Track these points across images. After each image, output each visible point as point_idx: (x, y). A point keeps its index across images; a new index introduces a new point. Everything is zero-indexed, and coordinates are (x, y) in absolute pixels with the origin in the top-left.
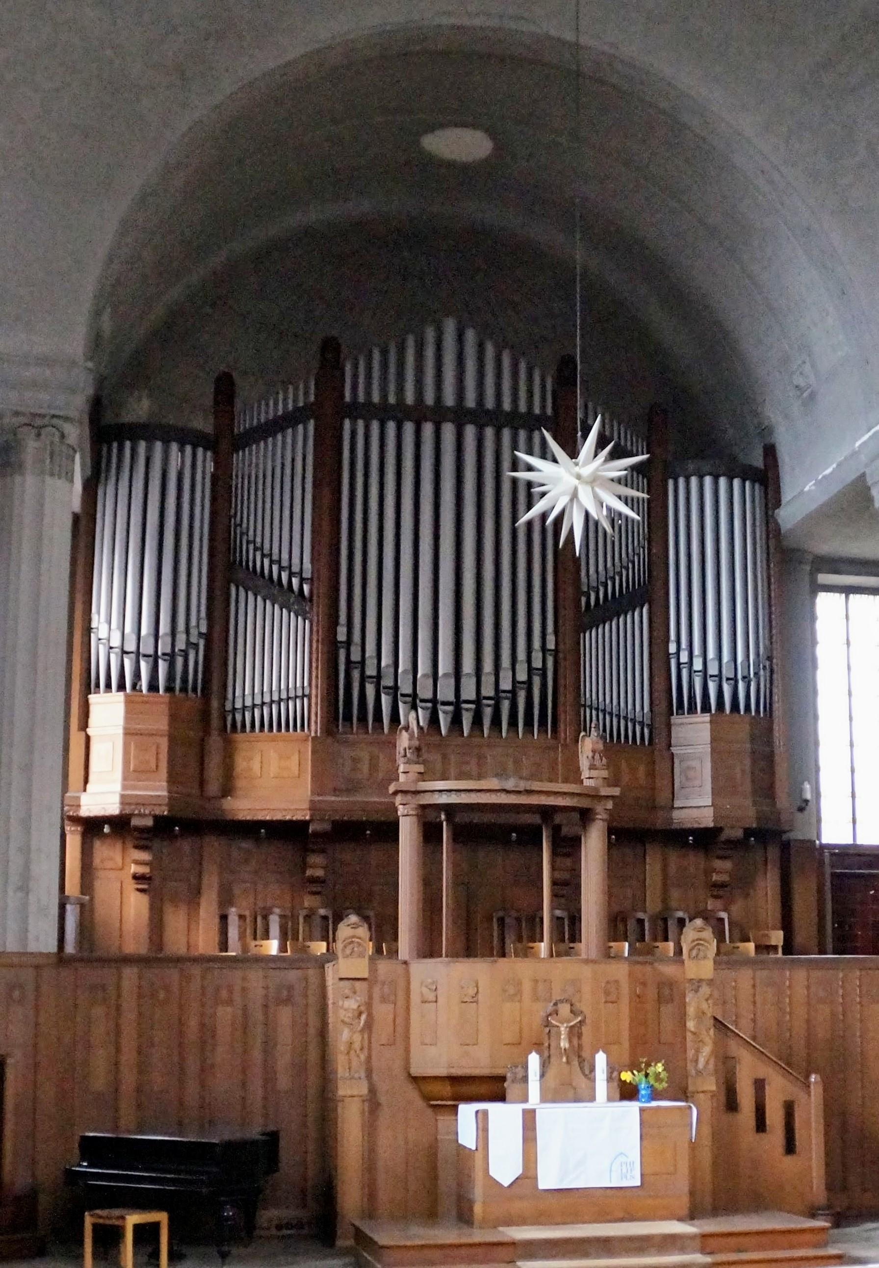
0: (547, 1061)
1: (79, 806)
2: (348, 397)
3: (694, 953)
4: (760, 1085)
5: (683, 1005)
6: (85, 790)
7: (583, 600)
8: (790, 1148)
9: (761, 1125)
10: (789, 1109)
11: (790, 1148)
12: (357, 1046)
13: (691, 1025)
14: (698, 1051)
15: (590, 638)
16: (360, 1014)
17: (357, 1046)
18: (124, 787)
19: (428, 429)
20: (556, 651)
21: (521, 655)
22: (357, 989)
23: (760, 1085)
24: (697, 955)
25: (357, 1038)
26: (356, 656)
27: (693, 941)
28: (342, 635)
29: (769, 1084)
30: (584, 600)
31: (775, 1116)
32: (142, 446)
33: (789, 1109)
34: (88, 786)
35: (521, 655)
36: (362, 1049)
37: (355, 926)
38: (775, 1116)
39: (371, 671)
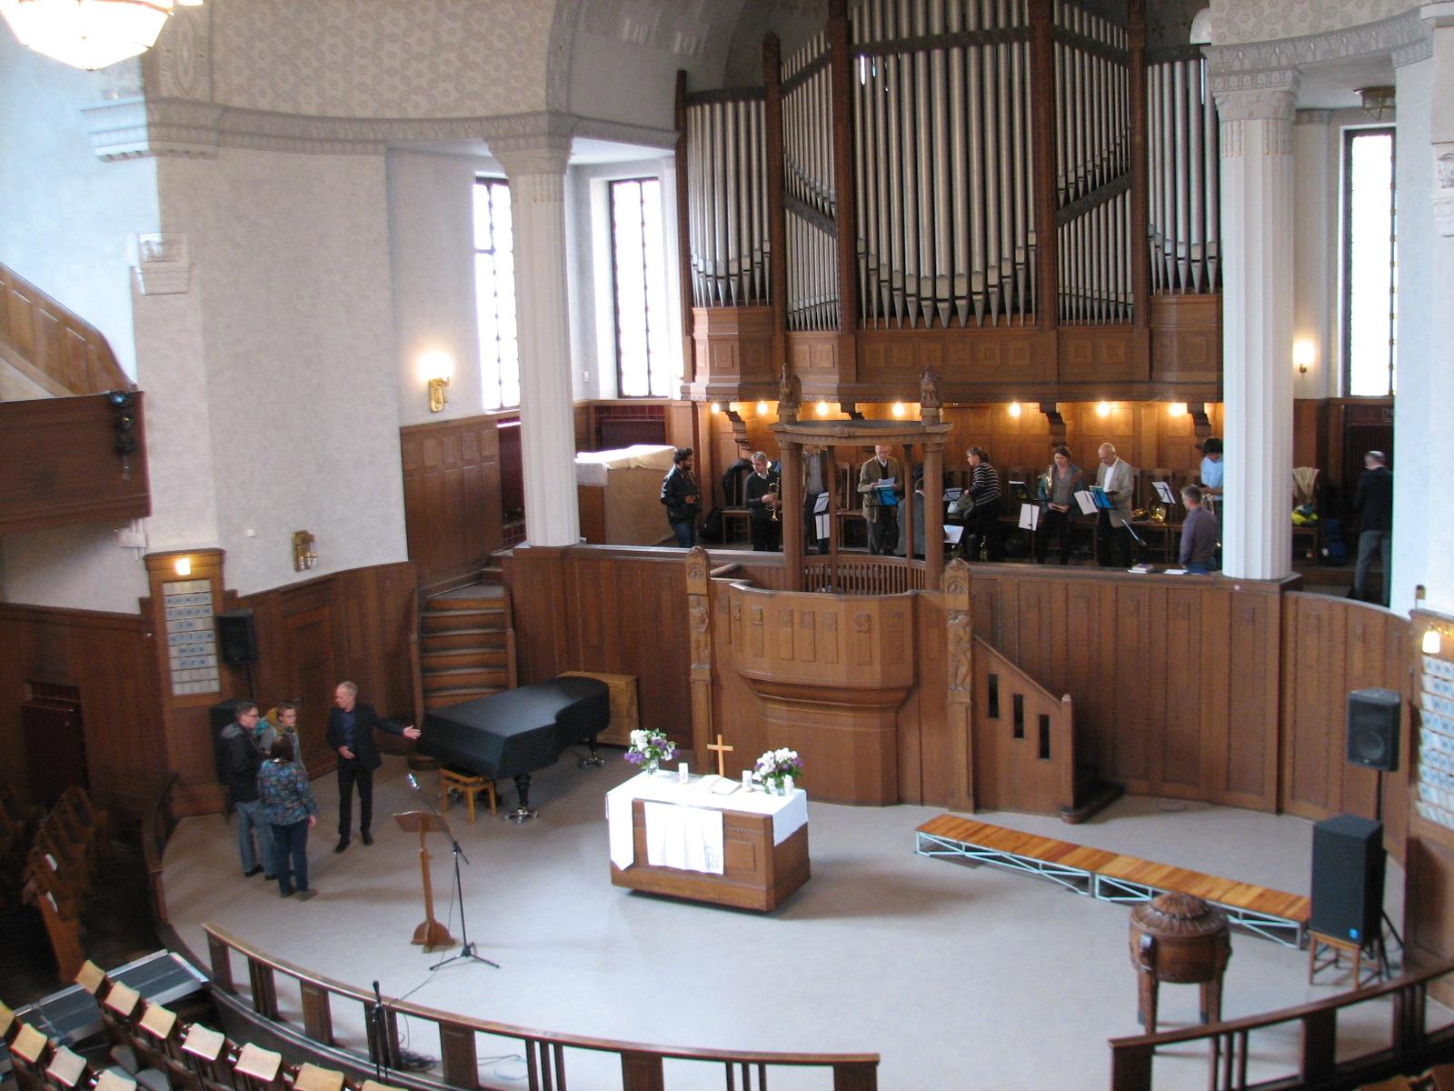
0: (761, 687)
1: (690, 393)
2: (763, 104)
3: (953, 587)
4: (1018, 701)
5: (945, 630)
6: (694, 380)
7: (1062, 197)
8: (1044, 752)
9: (1019, 733)
10: (1044, 722)
11: (1044, 752)
12: (702, 644)
13: (951, 647)
14: (957, 669)
15: (1067, 233)
16: (703, 622)
17: (702, 644)
18: (711, 381)
19: (937, 55)
20: (771, 253)
21: (1006, 253)
22: (702, 602)
23: (1018, 701)
24: (956, 589)
25: (702, 638)
26: (873, 265)
27: (950, 578)
28: (861, 248)
29: (670, 777)
30: (1062, 197)
31: (1031, 725)
32: (718, 107)
33: (1044, 722)
34: (697, 377)
35: (1006, 253)
36: (706, 646)
37: (957, 568)
38: (1031, 725)
39: (884, 275)
